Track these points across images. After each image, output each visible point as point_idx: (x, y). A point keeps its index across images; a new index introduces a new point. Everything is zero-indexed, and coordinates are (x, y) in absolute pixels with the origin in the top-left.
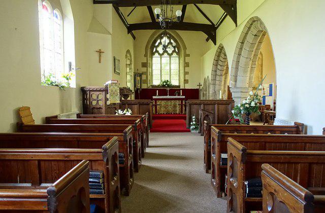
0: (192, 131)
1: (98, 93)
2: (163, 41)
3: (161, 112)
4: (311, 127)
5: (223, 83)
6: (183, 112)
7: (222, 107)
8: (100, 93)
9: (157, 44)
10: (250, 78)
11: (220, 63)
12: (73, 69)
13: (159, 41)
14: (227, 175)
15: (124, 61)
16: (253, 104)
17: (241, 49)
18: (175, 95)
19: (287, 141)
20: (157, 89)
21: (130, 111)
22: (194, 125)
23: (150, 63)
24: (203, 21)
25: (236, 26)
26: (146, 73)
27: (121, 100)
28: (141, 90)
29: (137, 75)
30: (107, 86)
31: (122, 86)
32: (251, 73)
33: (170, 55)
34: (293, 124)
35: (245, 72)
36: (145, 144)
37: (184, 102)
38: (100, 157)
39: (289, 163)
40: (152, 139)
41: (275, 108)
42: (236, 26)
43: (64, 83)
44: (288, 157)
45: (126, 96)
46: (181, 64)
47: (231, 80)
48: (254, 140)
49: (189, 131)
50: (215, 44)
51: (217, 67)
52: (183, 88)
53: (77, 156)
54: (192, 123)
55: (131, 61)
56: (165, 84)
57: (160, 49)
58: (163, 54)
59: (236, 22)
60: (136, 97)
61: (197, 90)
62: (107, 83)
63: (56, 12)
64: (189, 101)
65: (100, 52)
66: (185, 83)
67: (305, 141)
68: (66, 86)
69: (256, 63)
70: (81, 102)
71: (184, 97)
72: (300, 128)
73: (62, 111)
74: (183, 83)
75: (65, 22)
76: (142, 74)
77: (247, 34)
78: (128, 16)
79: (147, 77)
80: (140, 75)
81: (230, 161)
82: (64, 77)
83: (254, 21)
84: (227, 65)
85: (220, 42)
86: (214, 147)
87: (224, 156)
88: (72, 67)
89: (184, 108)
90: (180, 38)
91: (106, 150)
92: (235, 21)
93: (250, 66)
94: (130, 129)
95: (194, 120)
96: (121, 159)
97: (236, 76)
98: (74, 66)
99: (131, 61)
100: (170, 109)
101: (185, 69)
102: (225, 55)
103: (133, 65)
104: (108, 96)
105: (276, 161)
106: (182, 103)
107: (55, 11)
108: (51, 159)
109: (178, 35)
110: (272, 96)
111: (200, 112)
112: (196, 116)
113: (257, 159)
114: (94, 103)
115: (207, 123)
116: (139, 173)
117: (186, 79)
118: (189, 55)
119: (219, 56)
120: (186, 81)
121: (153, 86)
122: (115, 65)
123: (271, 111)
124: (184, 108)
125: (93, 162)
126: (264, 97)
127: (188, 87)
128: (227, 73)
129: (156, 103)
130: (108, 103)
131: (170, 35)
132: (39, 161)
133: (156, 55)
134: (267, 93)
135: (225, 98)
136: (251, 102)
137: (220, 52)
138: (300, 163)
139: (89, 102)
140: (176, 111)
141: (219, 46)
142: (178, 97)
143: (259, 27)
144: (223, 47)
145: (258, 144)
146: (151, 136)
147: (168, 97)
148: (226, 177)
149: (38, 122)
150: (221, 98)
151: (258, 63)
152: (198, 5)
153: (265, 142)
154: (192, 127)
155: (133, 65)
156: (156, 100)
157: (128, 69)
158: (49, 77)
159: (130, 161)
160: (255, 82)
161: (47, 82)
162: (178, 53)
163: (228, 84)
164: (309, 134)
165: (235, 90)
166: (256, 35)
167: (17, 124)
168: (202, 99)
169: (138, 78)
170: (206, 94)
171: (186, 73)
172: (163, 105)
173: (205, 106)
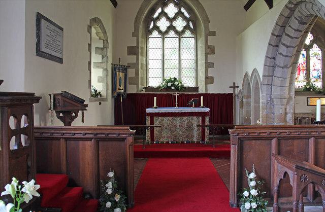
9: (156, 15)
13: (159, 10)
20: (155, 95)
26: (135, 66)
33: (180, 34)
54: (246, 194)
55: (105, 41)
56: (169, 84)
57: (163, 24)
66: (207, 83)
71: (208, 110)
76: (129, 66)
79: (137, 73)
80: (125, 70)
99: (105, 41)
100: (181, 135)
118: (213, 34)
119: (283, 27)
120: (209, 80)
121: (149, 89)
122: (38, 36)
127: (213, 90)
129: (152, 122)
133: (155, 33)
140: (193, 136)
154: (247, 205)
156: (152, 115)
162: (194, 31)
170: (248, 104)
171: (208, 65)
173: (283, 142)
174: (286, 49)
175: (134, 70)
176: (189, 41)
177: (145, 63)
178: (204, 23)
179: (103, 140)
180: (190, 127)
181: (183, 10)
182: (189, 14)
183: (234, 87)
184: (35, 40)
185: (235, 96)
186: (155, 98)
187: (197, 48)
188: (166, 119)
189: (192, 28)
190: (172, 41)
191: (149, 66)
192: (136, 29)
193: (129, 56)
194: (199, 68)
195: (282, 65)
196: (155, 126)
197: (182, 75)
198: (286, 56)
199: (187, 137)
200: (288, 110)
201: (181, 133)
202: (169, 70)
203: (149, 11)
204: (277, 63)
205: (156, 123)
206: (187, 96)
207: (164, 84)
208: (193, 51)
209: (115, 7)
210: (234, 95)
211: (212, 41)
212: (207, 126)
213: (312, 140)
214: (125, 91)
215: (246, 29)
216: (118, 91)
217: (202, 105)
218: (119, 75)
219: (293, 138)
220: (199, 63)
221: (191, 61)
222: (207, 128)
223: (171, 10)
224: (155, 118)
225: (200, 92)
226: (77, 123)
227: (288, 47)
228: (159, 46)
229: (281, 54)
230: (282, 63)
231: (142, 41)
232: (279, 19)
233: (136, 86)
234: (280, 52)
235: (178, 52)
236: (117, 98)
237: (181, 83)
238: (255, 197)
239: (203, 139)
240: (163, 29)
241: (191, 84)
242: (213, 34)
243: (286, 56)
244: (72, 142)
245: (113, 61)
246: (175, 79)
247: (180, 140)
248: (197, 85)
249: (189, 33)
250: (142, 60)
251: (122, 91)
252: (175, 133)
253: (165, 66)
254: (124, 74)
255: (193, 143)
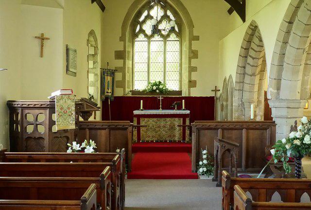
9: (142, 19)
13: (145, 14)
20: (142, 98)
26: (122, 69)
33: (165, 38)
54: (201, 163)
55: (96, 48)
56: (155, 88)
57: (148, 27)
71: (188, 112)
76: (116, 70)
80: (112, 73)
100: (164, 134)
118: (197, 38)
120: (192, 84)
122: (67, 60)
127: (196, 93)
129: (139, 122)
133: (141, 37)
140: (174, 136)
162: (179, 34)
171: (192, 69)
174: (252, 60)
176: (173, 45)
177: (131, 67)
178: (189, 28)
180: (172, 128)
181: (169, 13)
182: (174, 17)
186: (142, 101)
189: (178, 31)
190: (157, 43)
192: (123, 34)
193: (114, 53)
195: (250, 73)
196: (142, 126)
197: (167, 78)
198: (252, 66)
199: (170, 136)
200: (257, 112)
201: (164, 132)
202: (154, 73)
203: (135, 14)
205: (143, 123)
206: (171, 100)
207: (149, 87)
208: (177, 54)
210: (215, 99)
211: (195, 45)
212: (186, 126)
214: (113, 94)
215: (226, 35)
216: (106, 94)
220: (183, 66)
221: (175, 64)
223: (157, 12)
224: (141, 120)
225: (183, 95)
226: (91, 119)
227: (253, 58)
228: (145, 50)
229: (249, 64)
232: (245, 36)
233: (123, 89)
234: (248, 62)
236: (105, 102)
238: (206, 165)
239: (184, 138)
241: (175, 87)
246: (160, 82)
247: (164, 138)
248: (181, 88)
249: (175, 36)
251: (110, 94)
252: (159, 132)
253: (151, 70)
254: (112, 78)
255: (175, 142)
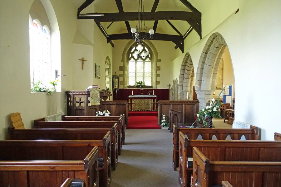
0: (163, 128)
1: (81, 96)
2: (138, 48)
3: (135, 109)
4: (265, 131)
5: (189, 85)
6: (155, 109)
7: (188, 107)
8: (83, 96)
9: (132, 51)
10: (213, 82)
11: (187, 68)
12: (59, 76)
13: (134, 48)
14: (192, 176)
15: (104, 66)
16: (215, 110)
17: (205, 58)
18: (148, 95)
19: (244, 146)
20: (133, 90)
21: (108, 111)
22: (165, 122)
23: (126, 67)
24: (172, 32)
25: (201, 38)
26: (123, 76)
27: (101, 102)
28: (118, 90)
29: (115, 78)
30: (88, 91)
31: (101, 89)
32: (213, 78)
33: (144, 60)
34: (249, 128)
35: (209, 77)
36: (121, 142)
37: (155, 101)
38: (82, 168)
39: (245, 172)
40: (127, 136)
41: (234, 106)
42: (201, 38)
43: (51, 88)
44: (244, 167)
45: (105, 98)
46: (153, 69)
47: (196, 83)
48: (216, 146)
49: (160, 128)
50: (183, 52)
51: (184, 71)
52: (155, 88)
53: (61, 168)
54: (162, 121)
55: (110, 65)
56: (139, 84)
57: (135, 55)
58: (138, 59)
59: (200, 35)
60: (114, 99)
61: (168, 90)
62: (89, 88)
63: (45, 28)
64: (160, 102)
65: (83, 60)
66: (156, 84)
67: (260, 146)
68: (53, 91)
69: (218, 70)
70: (66, 104)
71: (156, 96)
72: (255, 131)
73: (49, 112)
74: (155, 84)
75: (52, 34)
76: (120, 76)
77: (210, 46)
78: (108, 28)
79: (124, 79)
80: (118, 78)
81: (195, 168)
82: (51, 83)
83: (216, 36)
84: (193, 70)
85: (187, 51)
86: (181, 150)
87: (190, 159)
88: (58, 74)
89: (155, 106)
90: (153, 46)
91: (87, 162)
92: (200, 34)
93: (212, 72)
94: (109, 135)
95: (164, 118)
96: (101, 163)
97: (200, 81)
98: (59, 73)
99: (110, 65)
100: (144, 107)
101: (156, 73)
102: (191, 62)
103: (111, 69)
104: (90, 99)
105: (234, 170)
106: (154, 101)
107: (44, 27)
108: (38, 170)
109: (151, 44)
110: (231, 95)
111: (170, 112)
112: (166, 115)
113: (218, 169)
114: (77, 105)
115: (175, 128)
116: (115, 171)
117: (158, 80)
118: (160, 61)
119: (186, 62)
120: (158, 83)
121: (128, 87)
122: (96, 71)
123: (230, 110)
124: (155, 106)
125: (76, 172)
126: (225, 96)
127: (159, 87)
128: (193, 76)
129: (131, 101)
130: (90, 105)
131: (144, 43)
132: (28, 172)
133: (132, 60)
134: (227, 93)
135: (191, 99)
136: (213, 108)
137: (187, 59)
138: (254, 172)
139: (73, 104)
140: (149, 108)
141: (186, 54)
142: (151, 96)
143: (221, 42)
144: (189, 55)
145: (219, 148)
146: (127, 132)
147: (142, 96)
148: (192, 177)
149: (27, 126)
150: (187, 99)
151: (220, 66)
152: (170, 20)
153: (225, 147)
154: (162, 124)
155: (111, 69)
156: (131, 99)
157: (107, 72)
158: (37, 85)
159: (109, 161)
160: (217, 84)
161: (36, 89)
162: (151, 59)
163: (194, 84)
164: (263, 140)
165: (200, 92)
166: (217, 48)
167: (9, 128)
168: (171, 100)
169: (116, 80)
170: (175, 93)
171: (157, 76)
172: (137, 103)
173: (174, 106)
175: (122, 78)
176: (148, 64)
177: (127, 74)
179: (118, 105)
180: (148, 104)
181: (146, 48)
182: (148, 50)
183: (169, 86)
184: (95, 73)
185: (170, 90)
186: (133, 91)
187: (152, 67)
188: (137, 100)
190: (140, 63)
191: (129, 76)
194: (153, 77)
198: (187, 74)
200: (190, 96)
201: (144, 106)
204: (185, 77)
205: (133, 102)
208: (150, 69)
209: (113, 47)
213: (183, 105)
215: (174, 59)
216: (115, 87)
217: (153, 94)
218: (116, 80)
219: (178, 104)
220: (153, 74)
222: (155, 104)
227: (188, 70)
229: (185, 73)
230: (186, 77)
231: (126, 64)
235: (143, 69)
237: (144, 84)
240: (136, 58)
242: (160, 61)
243: (187, 74)
244: (109, 106)
245: (113, 74)
246: (142, 82)
250: (126, 73)
251: (117, 88)
